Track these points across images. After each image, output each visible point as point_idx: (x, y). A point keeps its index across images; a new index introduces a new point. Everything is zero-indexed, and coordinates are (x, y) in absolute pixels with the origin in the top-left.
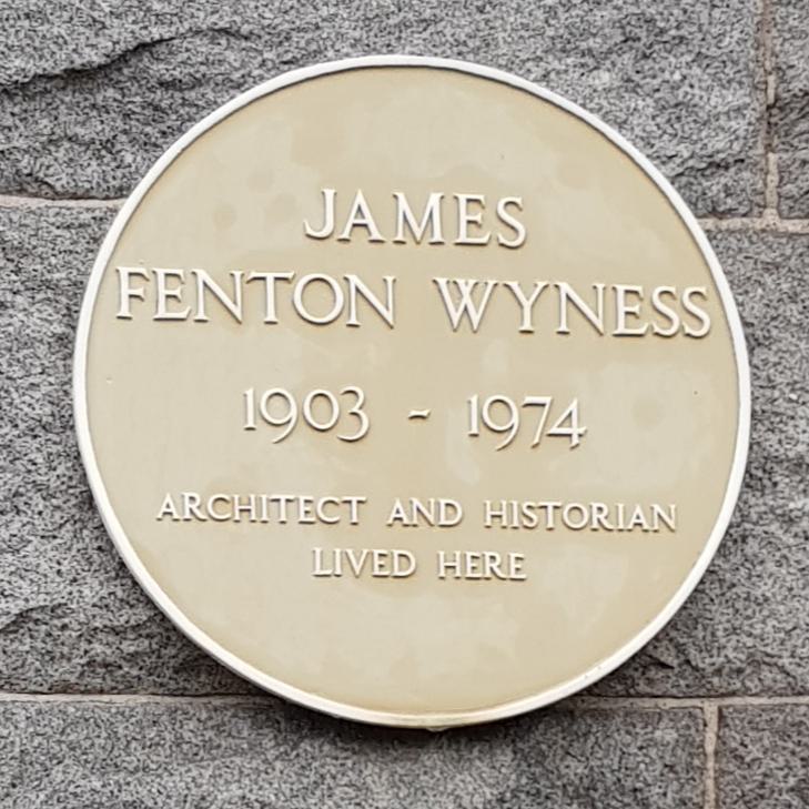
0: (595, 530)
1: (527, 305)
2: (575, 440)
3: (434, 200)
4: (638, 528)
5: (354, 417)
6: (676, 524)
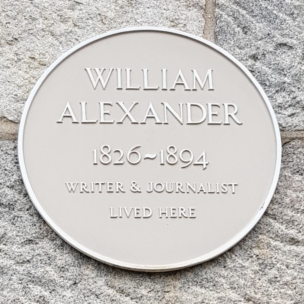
0: (177, 192)
2: (205, 166)
3: (209, 72)
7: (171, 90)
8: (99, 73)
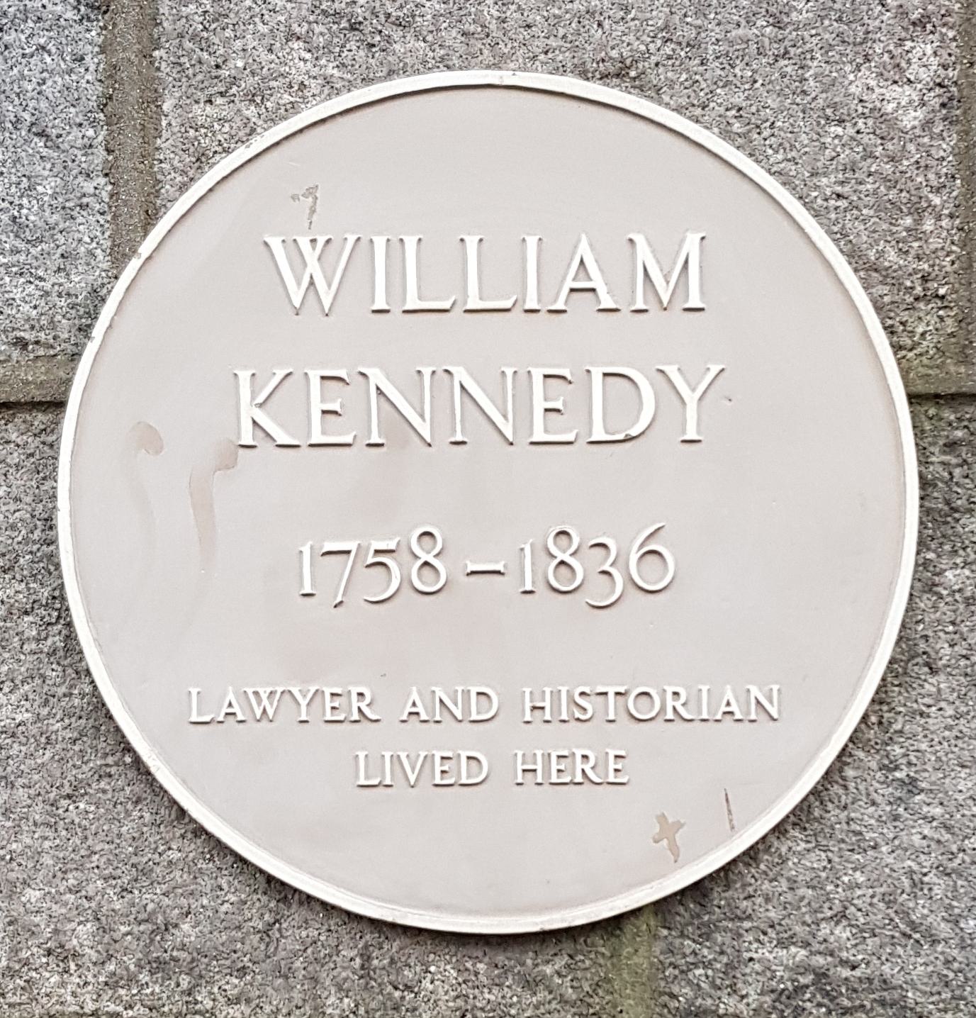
1: (691, 398)
3: (691, 245)
4: (728, 717)
5: (605, 577)
6: (779, 712)
7: (551, 311)
8: (311, 256)
